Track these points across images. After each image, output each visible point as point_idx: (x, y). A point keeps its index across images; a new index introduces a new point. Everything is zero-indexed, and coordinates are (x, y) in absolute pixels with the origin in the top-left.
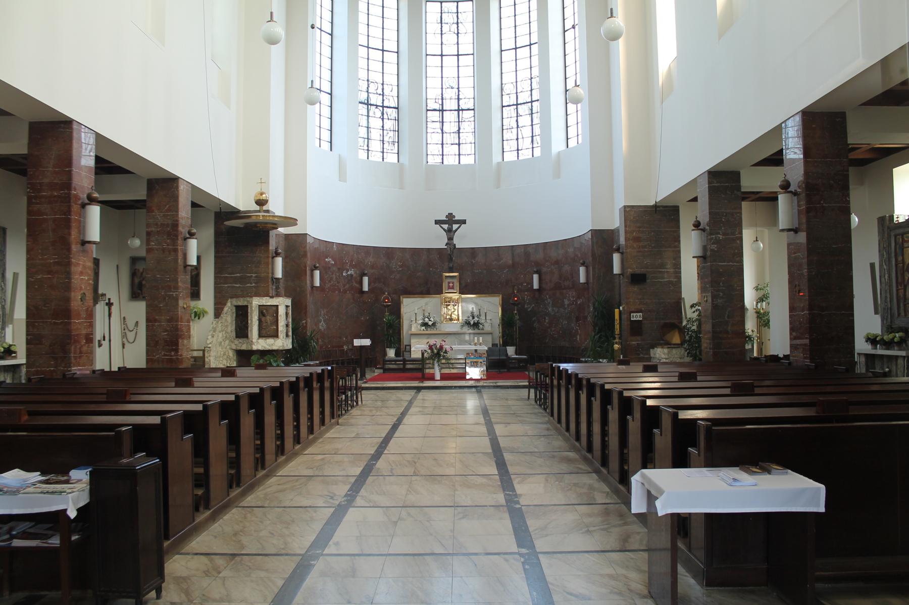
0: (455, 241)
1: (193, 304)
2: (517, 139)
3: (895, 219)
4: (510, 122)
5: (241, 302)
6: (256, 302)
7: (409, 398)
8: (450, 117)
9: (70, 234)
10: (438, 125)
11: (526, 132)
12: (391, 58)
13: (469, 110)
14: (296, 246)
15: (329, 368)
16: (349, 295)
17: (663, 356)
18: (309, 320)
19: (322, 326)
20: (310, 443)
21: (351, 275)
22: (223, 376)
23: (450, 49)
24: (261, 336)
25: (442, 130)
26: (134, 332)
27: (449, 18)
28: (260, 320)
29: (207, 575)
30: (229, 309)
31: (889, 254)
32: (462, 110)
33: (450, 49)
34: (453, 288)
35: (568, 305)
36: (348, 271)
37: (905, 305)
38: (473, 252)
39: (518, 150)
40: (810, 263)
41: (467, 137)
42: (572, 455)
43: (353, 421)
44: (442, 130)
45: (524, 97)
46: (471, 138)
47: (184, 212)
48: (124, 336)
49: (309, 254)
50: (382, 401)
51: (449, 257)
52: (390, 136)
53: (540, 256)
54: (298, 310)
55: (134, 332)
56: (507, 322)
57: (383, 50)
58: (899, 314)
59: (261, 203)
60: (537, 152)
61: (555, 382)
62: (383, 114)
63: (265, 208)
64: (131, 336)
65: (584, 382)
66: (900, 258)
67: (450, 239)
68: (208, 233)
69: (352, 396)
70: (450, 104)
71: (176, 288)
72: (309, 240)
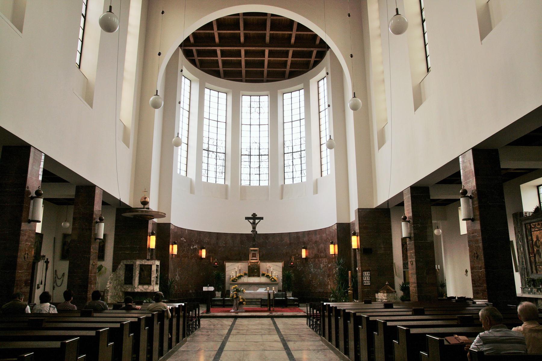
0: (257, 229)
1: (99, 263)
3: (524, 215)
4: (288, 162)
5: (129, 262)
6: (138, 262)
8: (255, 159)
9: (21, 216)
10: (248, 163)
11: (298, 168)
12: (222, 126)
14: (165, 232)
15: (183, 304)
16: (193, 261)
19: (177, 278)
21: (196, 248)
22: (114, 309)
23: (255, 121)
24: (140, 283)
26: (61, 280)
27: (255, 105)
28: (140, 273)
31: (522, 235)
33: (255, 121)
34: (255, 257)
37: (536, 267)
38: (266, 236)
40: (483, 239)
41: (265, 170)
46: (266, 171)
47: (98, 207)
48: (55, 282)
50: (214, 325)
51: (254, 238)
52: (221, 169)
54: (164, 269)
55: (61, 280)
56: (286, 278)
57: (218, 121)
58: (532, 272)
59: (145, 203)
60: (304, 179)
61: (326, 314)
62: (216, 156)
63: (146, 206)
64: (59, 282)
66: (529, 238)
67: (254, 228)
68: (112, 219)
70: (255, 152)
71: (89, 252)
72: (172, 227)
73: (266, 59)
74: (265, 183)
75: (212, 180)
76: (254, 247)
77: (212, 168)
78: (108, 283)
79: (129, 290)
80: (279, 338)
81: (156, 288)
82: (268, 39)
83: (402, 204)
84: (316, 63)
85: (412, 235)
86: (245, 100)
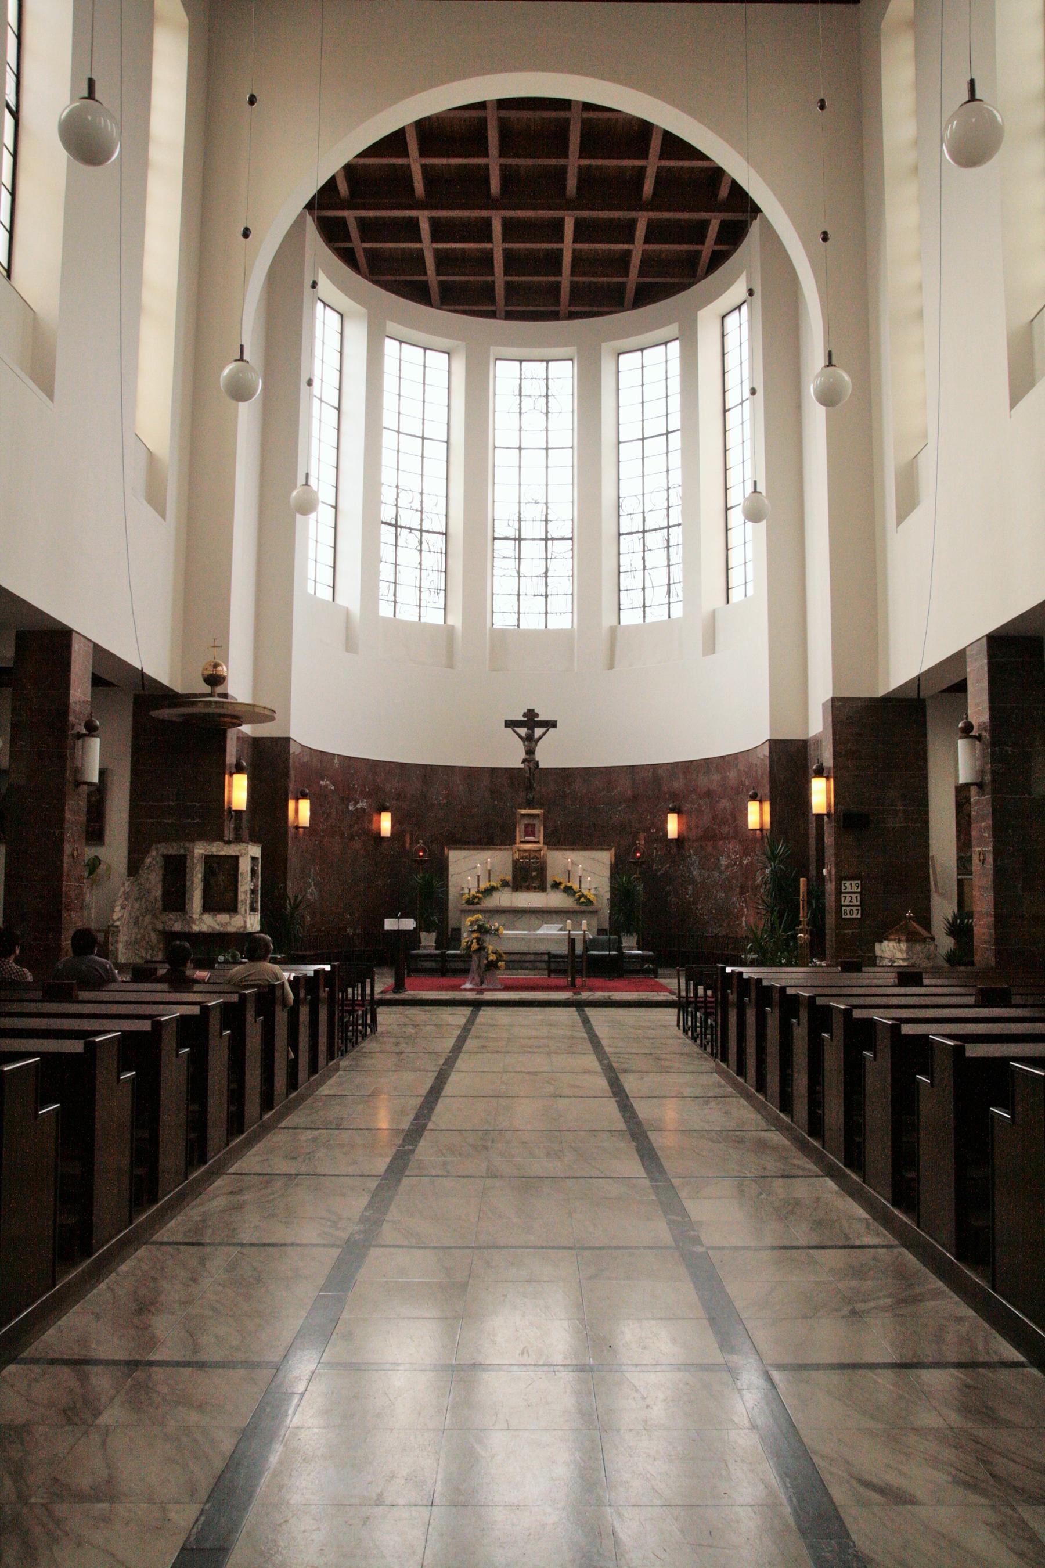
0: (538, 756)
1: (90, 852)
2: (643, 589)
5: (173, 850)
6: (200, 850)
7: (462, 1021)
8: (532, 550)
10: (513, 564)
11: (659, 577)
13: (563, 539)
14: (271, 762)
16: (357, 844)
17: (899, 955)
18: (290, 884)
19: (312, 893)
20: (290, 1108)
25: (519, 572)
27: (534, 388)
28: (206, 881)
29: (70, 1422)
30: (153, 859)
32: (553, 539)
34: (533, 834)
35: (727, 867)
36: (357, 803)
38: (566, 775)
39: (644, 606)
42: (776, 1138)
43: (367, 1062)
44: (519, 572)
45: (656, 519)
47: (80, 690)
49: (292, 773)
50: (415, 1026)
51: (529, 782)
53: (678, 785)
54: (273, 866)
57: (423, 438)
59: (215, 680)
60: (677, 611)
63: (219, 690)
65: (776, 996)
67: (530, 752)
68: (120, 726)
69: (364, 1015)
70: (533, 529)
72: (293, 749)
73: (568, 247)
74: (562, 621)
75: (407, 613)
76: (530, 804)
77: (408, 576)
78: (117, 908)
79: (177, 927)
80: (596, 1064)
81: (253, 923)
82: (572, 183)
83: (961, 687)
84: (718, 259)
85: (988, 778)
86: (505, 373)
